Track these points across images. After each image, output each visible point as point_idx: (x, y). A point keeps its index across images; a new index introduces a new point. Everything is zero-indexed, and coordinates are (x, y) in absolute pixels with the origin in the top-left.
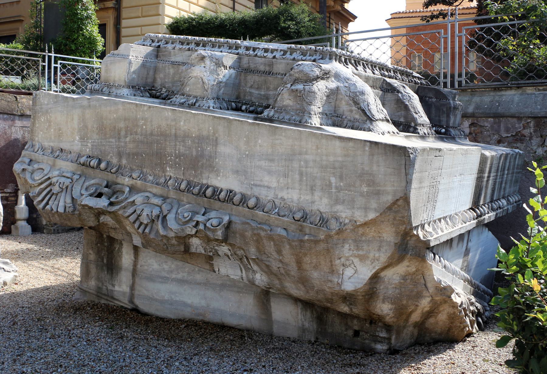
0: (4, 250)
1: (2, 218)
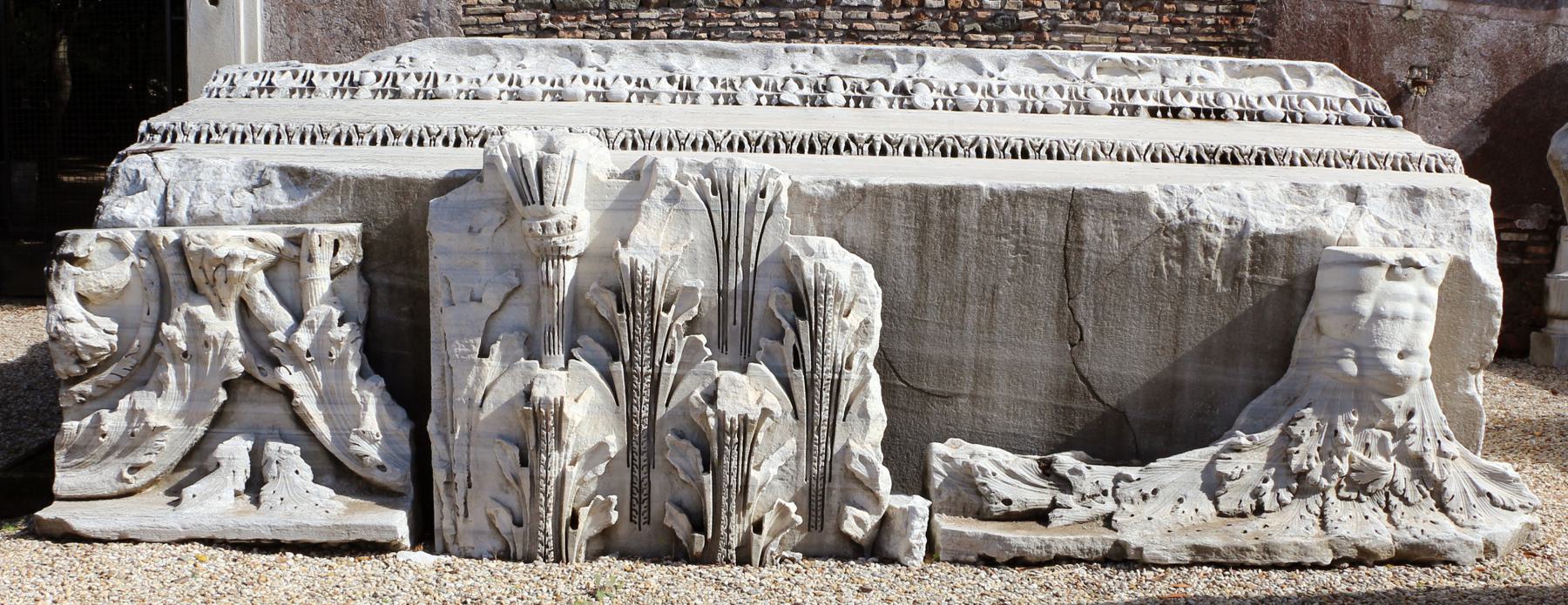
0: (1502, 414)
1: (1498, 323)
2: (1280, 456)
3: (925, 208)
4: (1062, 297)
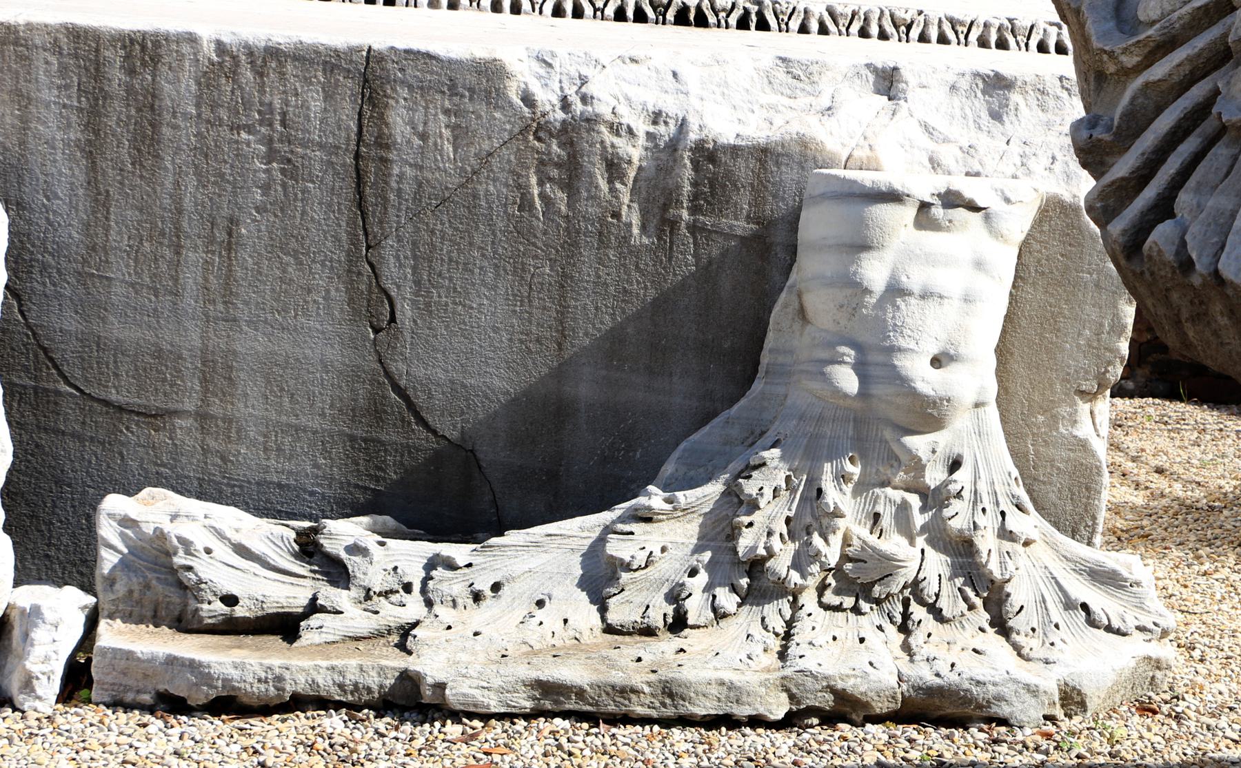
2: (720, 533)
3: (97, 70)
4: (354, 242)
